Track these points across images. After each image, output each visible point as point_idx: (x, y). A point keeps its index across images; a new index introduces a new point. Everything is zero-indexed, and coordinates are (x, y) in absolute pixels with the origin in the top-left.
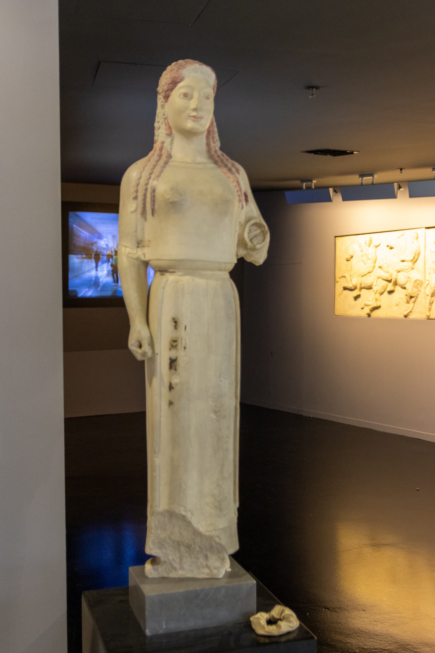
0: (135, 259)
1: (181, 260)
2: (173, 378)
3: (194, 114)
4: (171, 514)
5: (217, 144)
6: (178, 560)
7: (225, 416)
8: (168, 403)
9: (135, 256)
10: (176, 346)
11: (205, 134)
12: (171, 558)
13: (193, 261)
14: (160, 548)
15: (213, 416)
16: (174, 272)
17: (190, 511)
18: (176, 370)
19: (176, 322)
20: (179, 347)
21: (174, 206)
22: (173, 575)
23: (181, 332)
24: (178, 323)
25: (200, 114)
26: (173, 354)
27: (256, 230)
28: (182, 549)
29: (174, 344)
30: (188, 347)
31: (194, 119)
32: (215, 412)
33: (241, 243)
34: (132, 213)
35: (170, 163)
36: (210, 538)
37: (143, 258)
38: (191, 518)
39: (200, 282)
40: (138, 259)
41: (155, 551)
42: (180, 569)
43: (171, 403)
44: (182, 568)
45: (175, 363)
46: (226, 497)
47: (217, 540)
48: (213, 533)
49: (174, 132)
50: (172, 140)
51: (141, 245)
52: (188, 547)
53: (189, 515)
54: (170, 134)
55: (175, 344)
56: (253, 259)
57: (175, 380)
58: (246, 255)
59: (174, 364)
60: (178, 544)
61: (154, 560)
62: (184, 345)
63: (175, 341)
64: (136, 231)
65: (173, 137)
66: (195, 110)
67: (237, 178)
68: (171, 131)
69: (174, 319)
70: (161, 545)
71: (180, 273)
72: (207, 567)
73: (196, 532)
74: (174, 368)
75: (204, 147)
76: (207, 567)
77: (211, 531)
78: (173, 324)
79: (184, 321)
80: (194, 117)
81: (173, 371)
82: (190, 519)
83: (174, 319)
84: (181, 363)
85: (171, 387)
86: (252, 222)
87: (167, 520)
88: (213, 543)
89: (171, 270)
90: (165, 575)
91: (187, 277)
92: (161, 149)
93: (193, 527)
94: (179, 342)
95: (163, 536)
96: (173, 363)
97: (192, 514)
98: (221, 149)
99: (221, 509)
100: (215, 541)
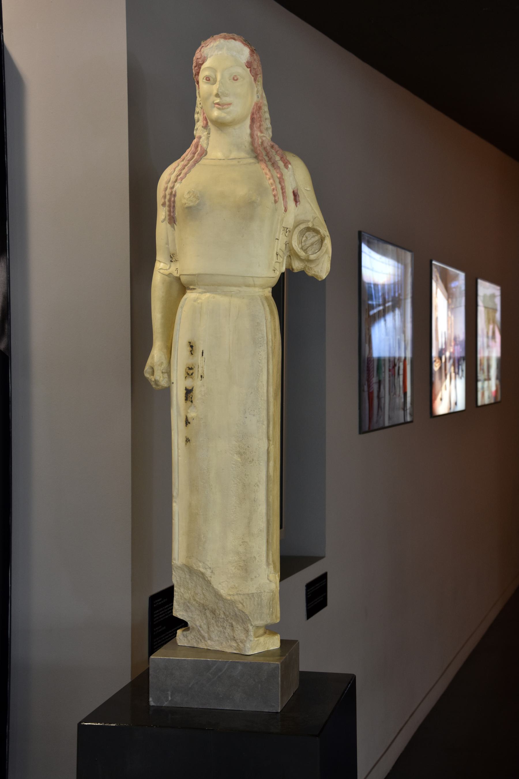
0: (167, 275)
1: (199, 275)
2: (189, 411)
3: (218, 100)
4: (190, 570)
5: (266, 135)
6: (205, 627)
7: (253, 460)
8: (184, 440)
9: (167, 272)
10: (192, 374)
11: (248, 122)
12: (198, 624)
13: (212, 275)
14: (186, 611)
15: (236, 457)
16: (194, 289)
17: (210, 568)
18: (192, 402)
19: (192, 347)
20: (195, 375)
21: (192, 211)
22: (202, 646)
23: (198, 359)
24: (194, 348)
25: (227, 100)
26: (189, 383)
27: (314, 236)
28: (208, 613)
29: (190, 372)
30: (205, 376)
31: (219, 106)
32: (240, 454)
33: (292, 254)
34: (162, 222)
35: (203, 161)
36: (232, 603)
37: (175, 274)
38: (211, 577)
39: (222, 300)
40: (170, 275)
41: (181, 613)
42: (209, 639)
43: (188, 440)
44: (210, 638)
45: (191, 394)
46: (255, 557)
47: (240, 606)
48: (236, 597)
49: (209, 124)
50: (209, 134)
51: (174, 260)
52: (213, 612)
53: (208, 573)
54: (206, 127)
55: (190, 372)
56: (313, 273)
57: (192, 414)
58: (305, 268)
59: (190, 395)
60: (203, 608)
61: (183, 624)
62: (200, 373)
63: (191, 369)
64: (167, 243)
65: (210, 130)
66: (217, 95)
67: (282, 175)
68: (207, 123)
69: (190, 343)
70: (187, 608)
71: (200, 290)
72: (234, 639)
73: (217, 595)
74: (190, 399)
75: (247, 139)
76: (234, 639)
77: (233, 595)
78: (189, 349)
79: (200, 347)
80: (218, 104)
81: (189, 403)
82: (209, 578)
83: (190, 343)
84: (197, 394)
85: (187, 422)
86: (302, 226)
87: (188, 576)
88: (236, 609)
89: (191, 287)
90: (195, 645)
91: (208, 295)
92: (197, 147)
93: (213, 588)
94: (195, 370)
95: (187, 596)
96: (189, 392)
97: (212, 572)
98: (273, 139)
99: (246, 571)
100: (237, 607)
